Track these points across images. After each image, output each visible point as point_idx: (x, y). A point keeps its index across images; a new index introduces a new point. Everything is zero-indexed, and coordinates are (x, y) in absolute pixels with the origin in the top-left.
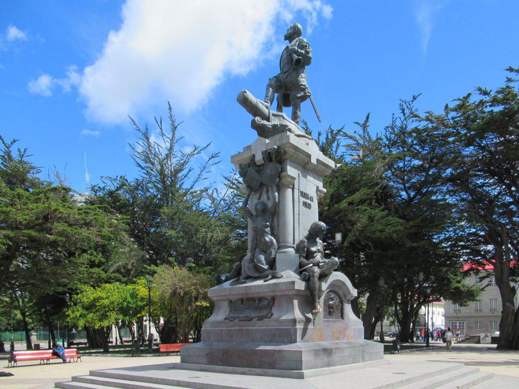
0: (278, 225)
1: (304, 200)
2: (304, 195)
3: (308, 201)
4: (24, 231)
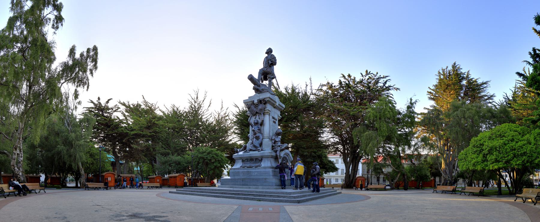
0: (263, 129)
2: (273, 118)
3: (275, 121)
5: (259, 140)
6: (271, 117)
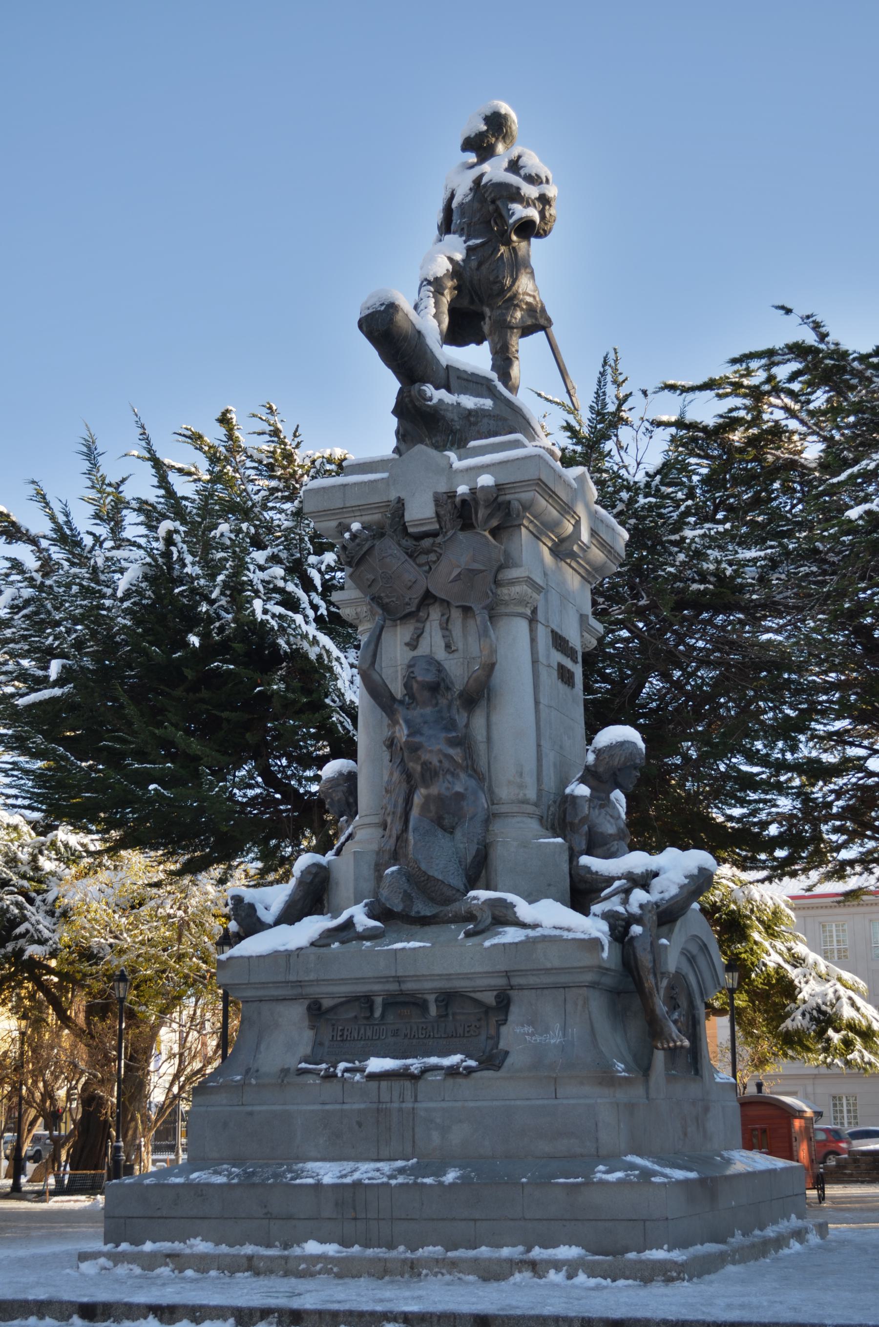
0: (489, 739)
2: (560, 642)
4: (831, 481)
5: (458, 834)
6: (543, 635)
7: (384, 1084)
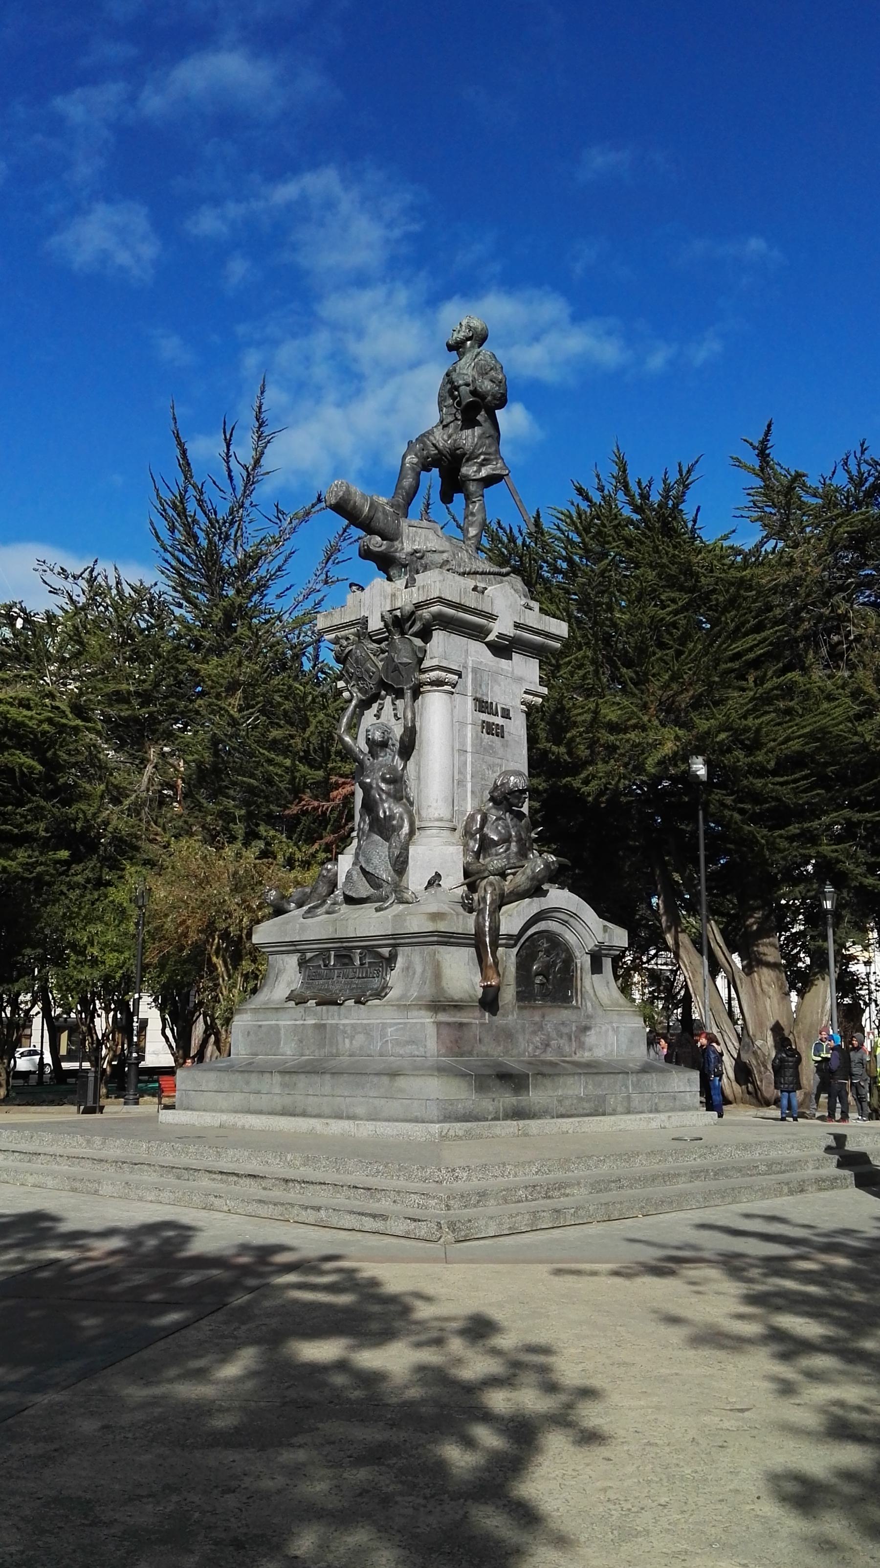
1: (485, 717)
2: (483, 706)
3: (499, 720)
7: (324, 1008)
